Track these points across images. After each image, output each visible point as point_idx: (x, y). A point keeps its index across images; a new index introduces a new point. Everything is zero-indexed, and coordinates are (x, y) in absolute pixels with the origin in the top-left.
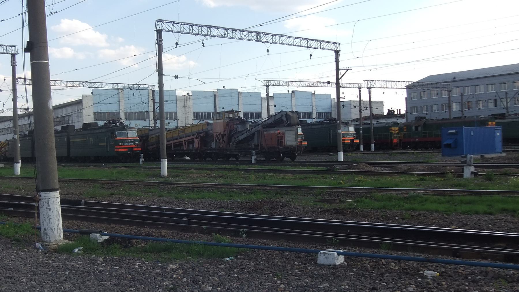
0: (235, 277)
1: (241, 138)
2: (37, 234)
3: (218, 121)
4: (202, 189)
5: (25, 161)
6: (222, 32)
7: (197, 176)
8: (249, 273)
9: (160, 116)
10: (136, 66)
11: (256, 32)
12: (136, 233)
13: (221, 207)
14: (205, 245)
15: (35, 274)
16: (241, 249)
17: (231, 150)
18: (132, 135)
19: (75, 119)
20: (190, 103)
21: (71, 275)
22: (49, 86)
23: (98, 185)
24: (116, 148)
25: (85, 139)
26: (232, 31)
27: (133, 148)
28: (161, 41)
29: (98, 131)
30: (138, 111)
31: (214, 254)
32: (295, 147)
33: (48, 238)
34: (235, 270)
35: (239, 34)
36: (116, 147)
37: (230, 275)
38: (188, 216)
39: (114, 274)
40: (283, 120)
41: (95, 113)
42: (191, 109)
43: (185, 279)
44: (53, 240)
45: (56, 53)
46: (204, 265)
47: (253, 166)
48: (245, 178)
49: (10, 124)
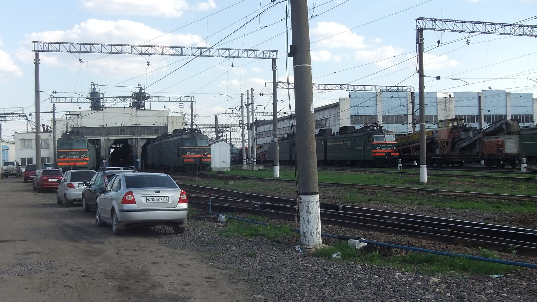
0: (504, 296)
1: (464, 145)
2: (296, 237)
3: (442, 129)
4: (465, 198)
5: (283, 163)
6: (489, 28)
7: (458, 183)
8: (521, 294)
9: (420, 119)
10: (394, 67)
11: (529, 26)
12: (395, 241)
13: (487, 219)
14: (471, 259)
15: (295, 276)
16: (511, 267)
17: (454, 156)
18: (390, 139)
19: (332, 123)
20: (452, 106)
21: (331, 281)
22: (311, 89)
23: (355, 190)
24: (373, 153)
25: (342, 143)
26: (500, 26)
27: (390, 153)
28: (422, 40)
29: (355, 135)
30: (396, 114)
31: (480, 269)
32: (515, 155)
33: (307, 241)
34: (505, 290)
35: (508, 29)
36: (373, 151)
37: (498, 294)
38: (450, 227)
39: (373, 282)
40: (501, 126)
41: (352, 116)
42: (453, 112)
43: (449, 294)
44: (311, 243)
45: (318, 57)
46: (469, 281)
47: (523, 175)
48: (514, 188)
49: (270, 127)
